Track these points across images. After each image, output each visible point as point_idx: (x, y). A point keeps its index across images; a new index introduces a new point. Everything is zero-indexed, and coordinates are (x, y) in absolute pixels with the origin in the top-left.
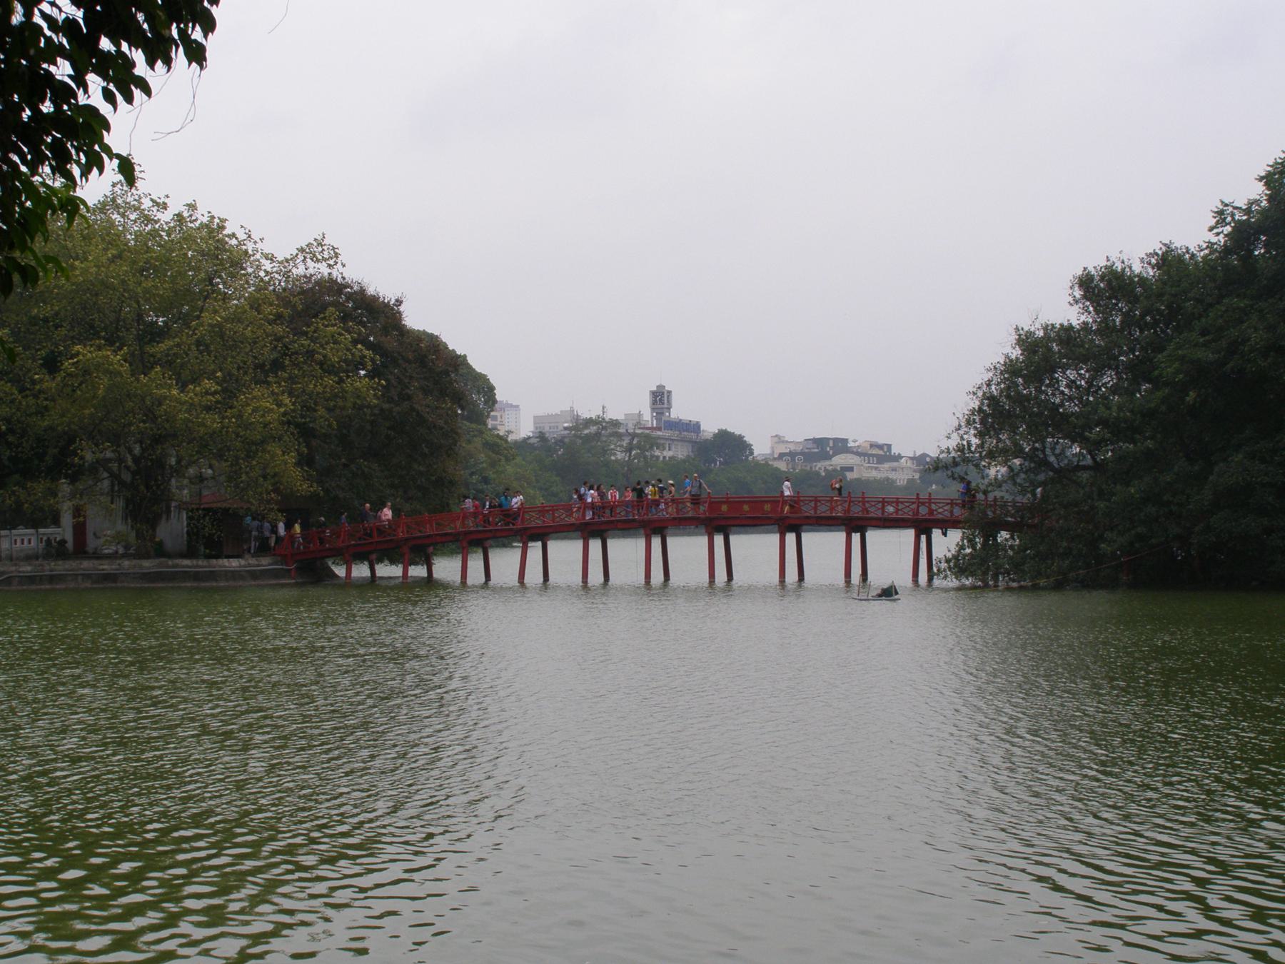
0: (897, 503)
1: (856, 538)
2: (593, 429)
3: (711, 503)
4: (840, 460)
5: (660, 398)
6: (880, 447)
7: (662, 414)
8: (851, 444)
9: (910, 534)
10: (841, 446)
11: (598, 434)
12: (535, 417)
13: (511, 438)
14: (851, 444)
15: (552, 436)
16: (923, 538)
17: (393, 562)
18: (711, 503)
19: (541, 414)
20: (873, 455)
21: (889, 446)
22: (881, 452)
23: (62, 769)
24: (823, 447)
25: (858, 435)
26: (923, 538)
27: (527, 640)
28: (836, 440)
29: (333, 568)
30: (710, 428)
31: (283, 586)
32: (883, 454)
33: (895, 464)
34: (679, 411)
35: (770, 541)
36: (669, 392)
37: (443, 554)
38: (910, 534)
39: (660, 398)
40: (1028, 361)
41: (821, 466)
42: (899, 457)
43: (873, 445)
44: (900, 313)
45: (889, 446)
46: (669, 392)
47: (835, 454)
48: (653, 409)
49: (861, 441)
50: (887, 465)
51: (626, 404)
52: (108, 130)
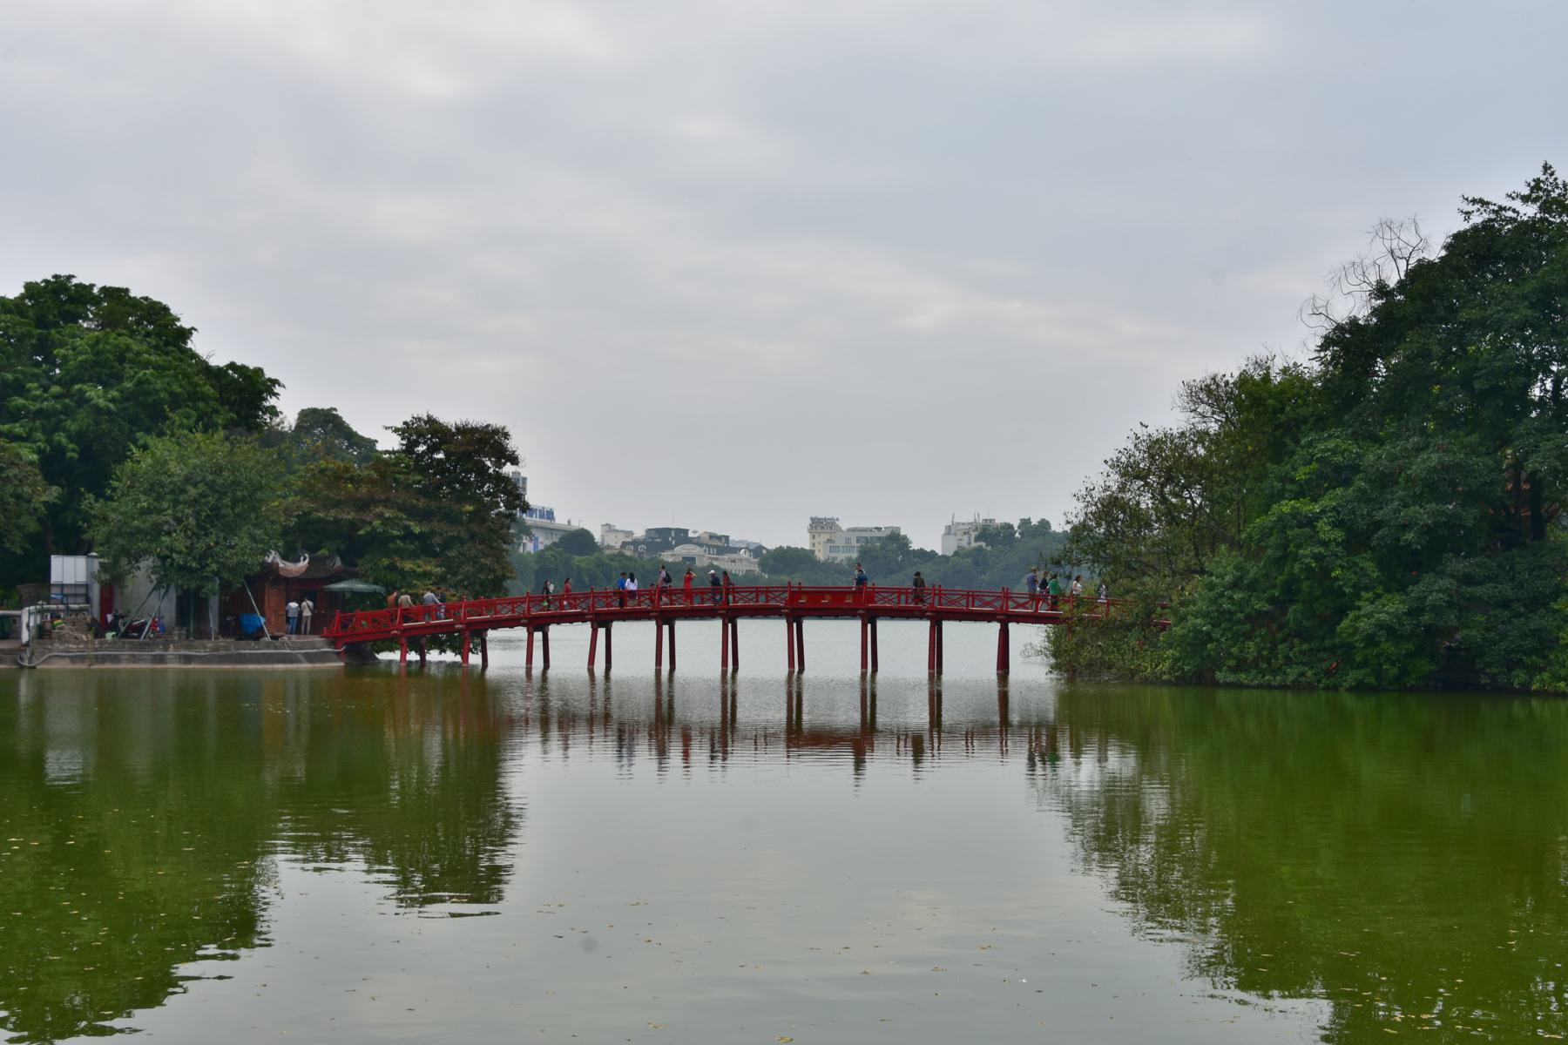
3: (792, 593)
4: (682, 550)
6: (719, 538)
8: (691, 535)
10: (682, 536)
12: (813, 519)
14: (691, 535)
16: (666, 628)
18: (792, 593)
19: (821, 516)
21: (727, 538)
23: (456, 737)
24: (663, 538)
25: (698, 526)
26: (666, 628)
28: (678, 531)
33: (733, 556)
35: (583, 630)
36: (525, 479)
38: (717, 624)
41: (667, 557)
42: (736, 550)
43: (712, 536)
44: (1066, 388)
50: (726, 557)
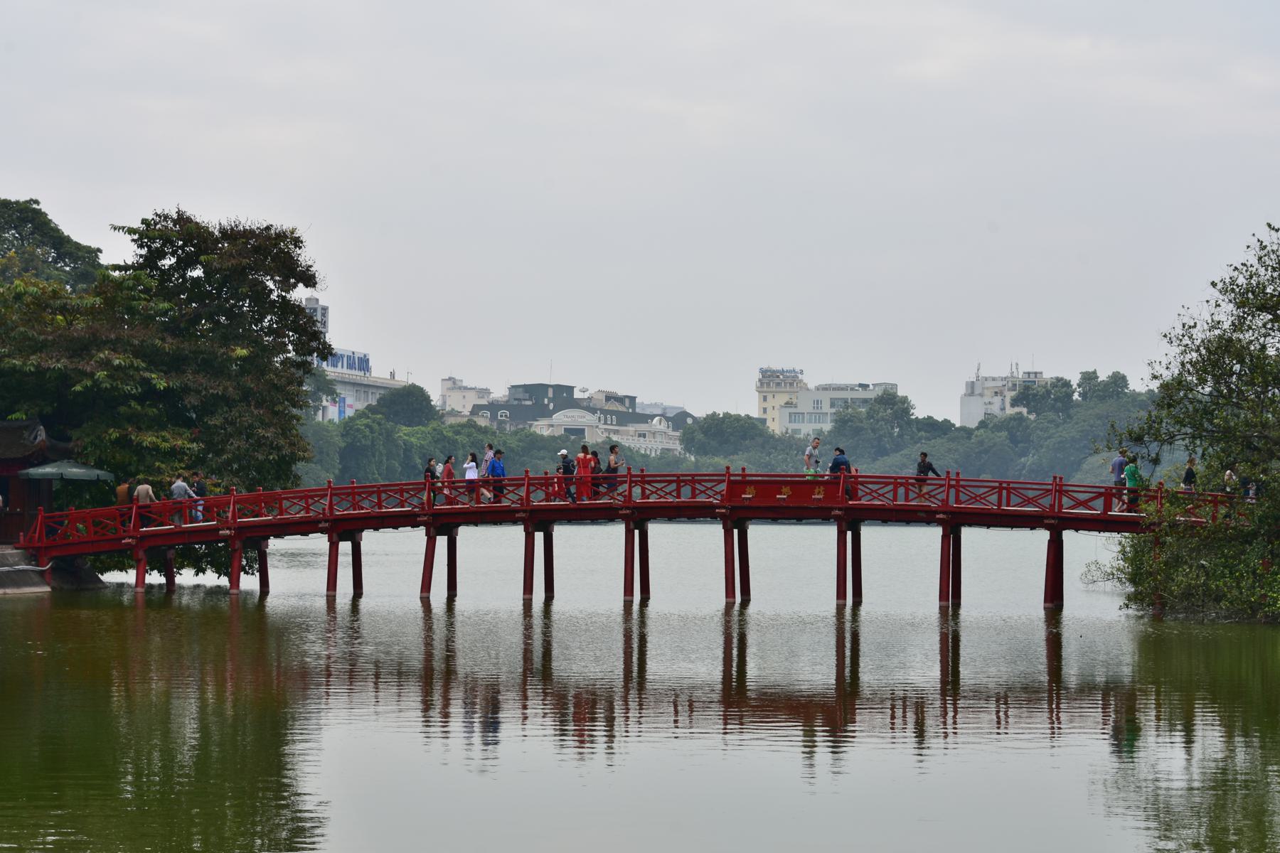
1: (345, 547)
6: (620, 400)
8: (577, 395)
10: (564, 396)
14: (577, 395)
17: (122, 568)
20: (612, 413)
21: (633, 399)
22: (621, 408)
24: (537, 399)
25: (588, 382)
28: (559, 389)
32: (623, 409)
33: (642, 427)
36: (325, 309)
37: (970, 525)
40: (1106, 384)
41: (542, 428)
42: (646, 418)
43: (610, 397)
45: (633, 399)
46: (325, 309)
47: (555, 410)
49: (592, 391)
50: (631, 428)
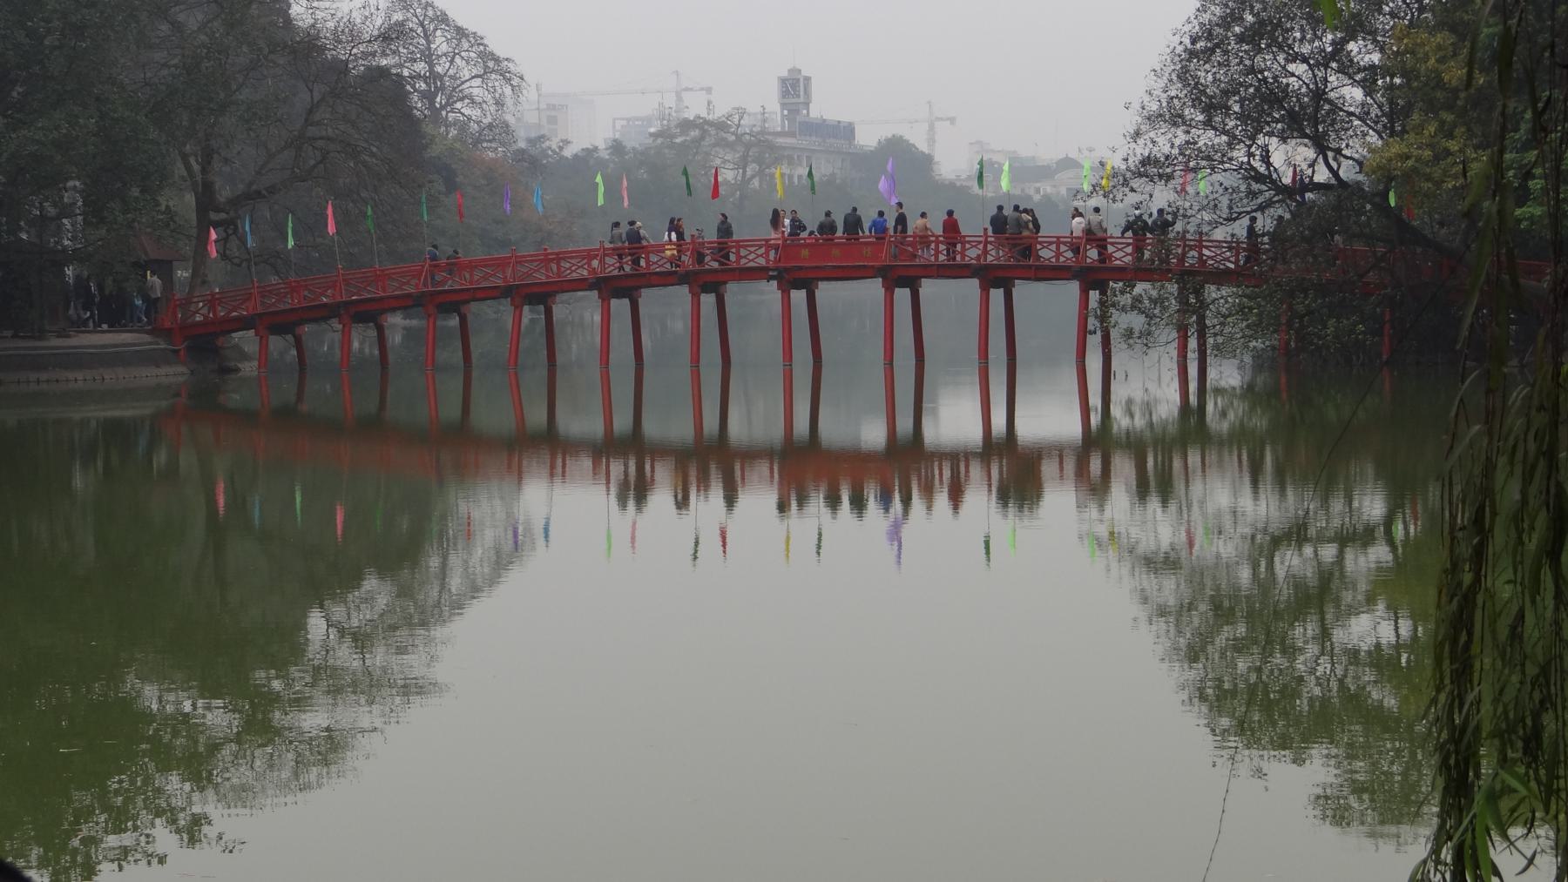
0: (1058, 244)
2: (695, 133)
5: (794, 88)
7: (797, 111)
9: (1074, 287)
11: (698, 141)
13: (568, 152)
15: (631, 143)
27: (584, 601)
29: (194, 223)
30: (868, 138)
31: (95, 347)
34: (823, 107)
36: (807, 79)
38: (1074, 287)
39: (794, 88)
46: (807, 79)
48: (783, 106)
51: (750, 97)
52: (1334, 810)
